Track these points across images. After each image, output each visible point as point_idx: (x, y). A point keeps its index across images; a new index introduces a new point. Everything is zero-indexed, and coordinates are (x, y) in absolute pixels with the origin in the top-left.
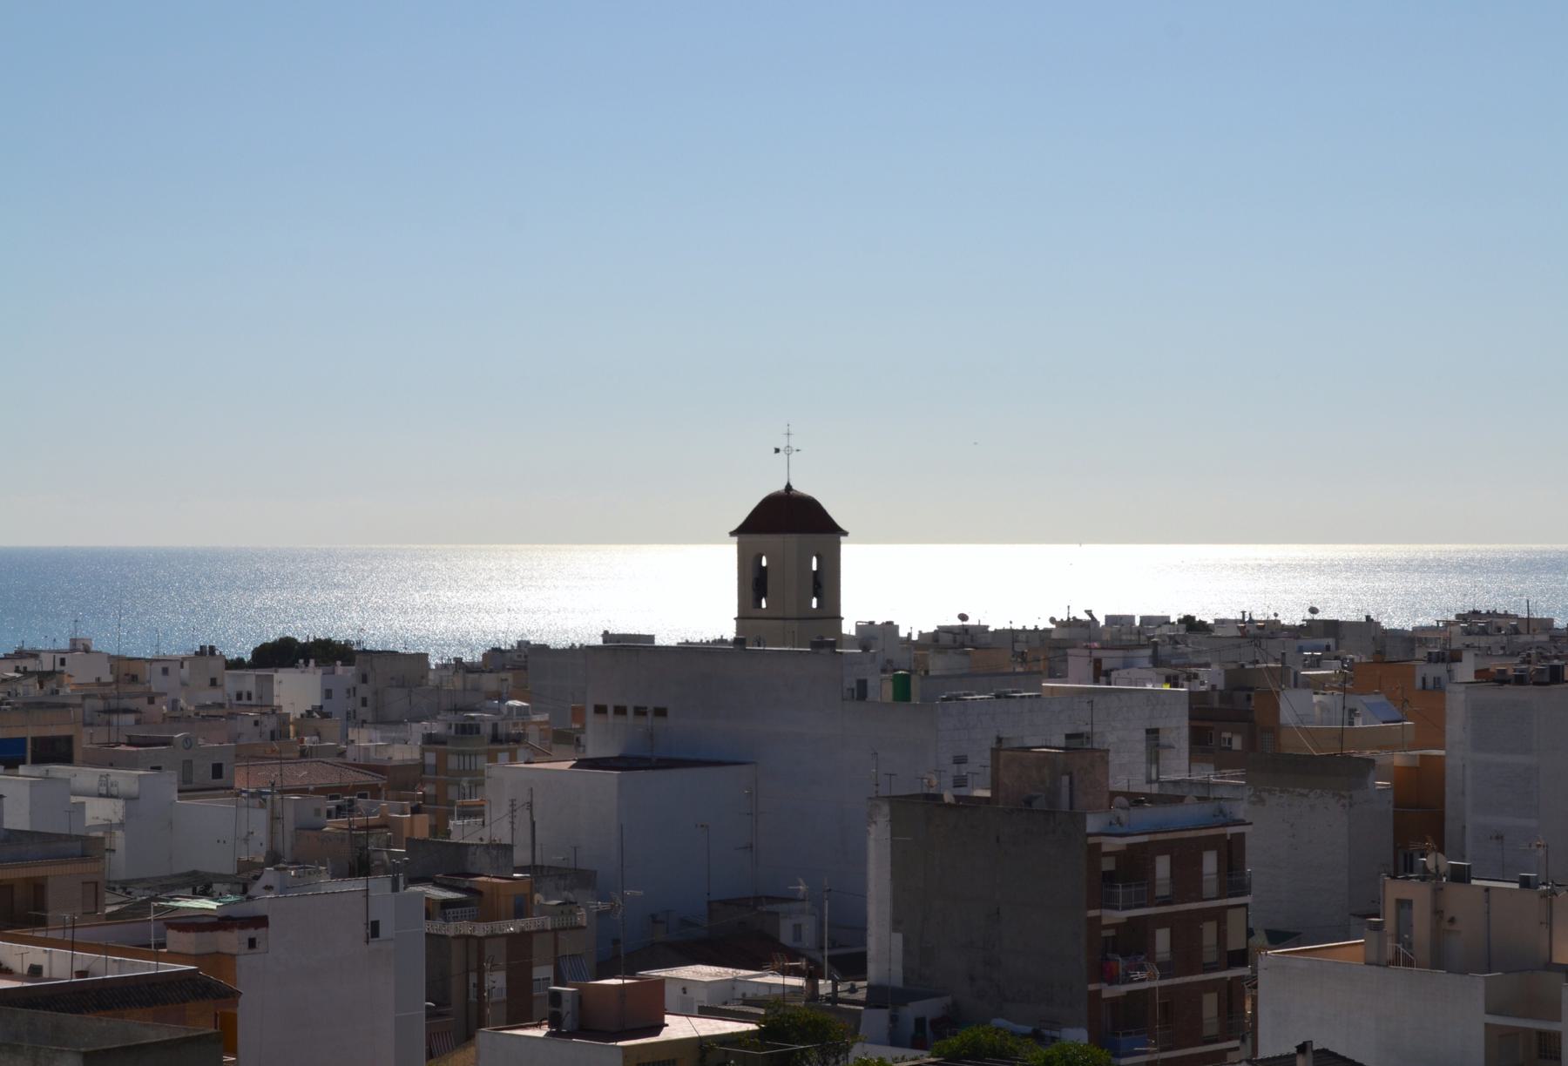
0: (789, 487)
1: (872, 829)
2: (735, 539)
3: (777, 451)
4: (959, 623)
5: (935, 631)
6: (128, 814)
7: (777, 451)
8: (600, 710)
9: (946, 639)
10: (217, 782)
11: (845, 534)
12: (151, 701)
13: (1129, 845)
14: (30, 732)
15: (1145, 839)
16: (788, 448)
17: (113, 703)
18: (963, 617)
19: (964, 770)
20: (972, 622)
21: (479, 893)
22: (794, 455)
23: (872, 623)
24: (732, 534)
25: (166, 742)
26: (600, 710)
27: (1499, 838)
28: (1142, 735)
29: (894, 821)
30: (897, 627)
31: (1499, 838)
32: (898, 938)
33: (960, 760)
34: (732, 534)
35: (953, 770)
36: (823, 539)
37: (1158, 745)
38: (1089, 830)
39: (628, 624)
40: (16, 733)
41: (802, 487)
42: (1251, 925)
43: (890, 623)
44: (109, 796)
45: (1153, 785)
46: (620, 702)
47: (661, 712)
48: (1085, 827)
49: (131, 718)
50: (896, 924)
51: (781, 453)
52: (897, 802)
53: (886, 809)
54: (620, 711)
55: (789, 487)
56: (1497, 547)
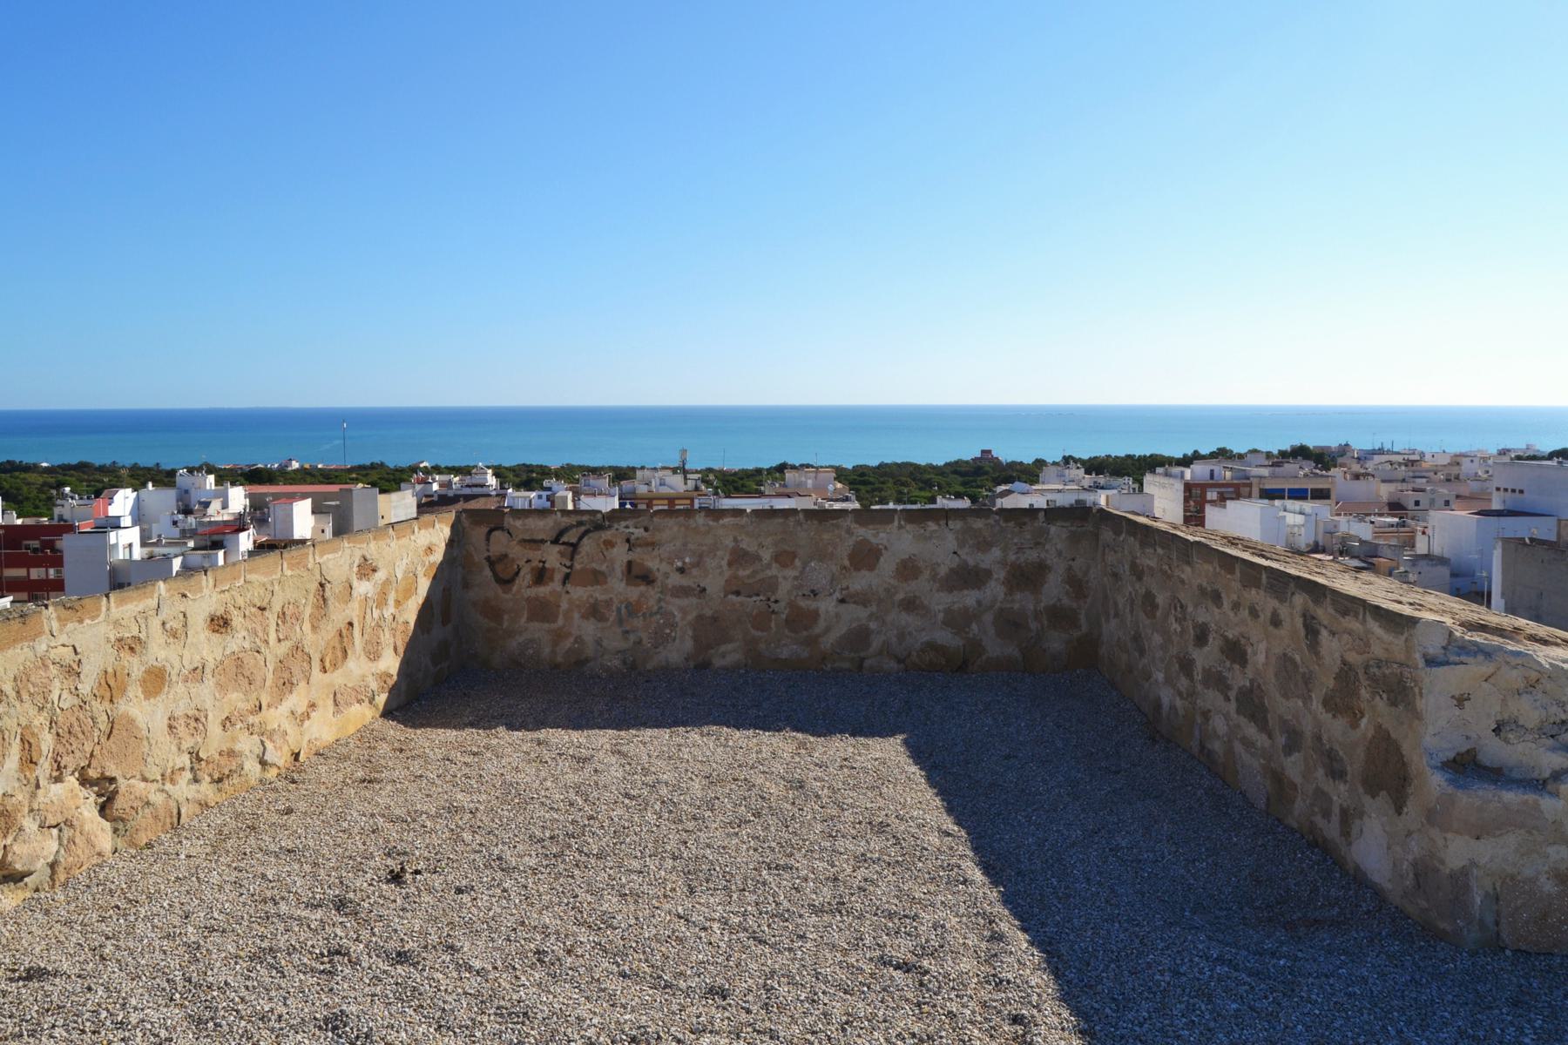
1: (1495, 552)
5: (975, 460)
6: (1306, 521)
8: (1498, 489)
10: (1417, 508)
12: (1436, 474)
14: (1287, 486)
17: (1417, 474)
21: (1374, 565)
25: (1423, 491)
26: (1498, 489)
29: (1504, 549)
32: (1503, 601)
39: (1131, 453)
40: (1305, 487)
44: (1301, 513)
45: (1425, 552)
47: (1521, 492)
49: (1424, 480)
50: (1503, 595)
52: (1506, 541)
53: (1500, 543)
54: (1506, 490)
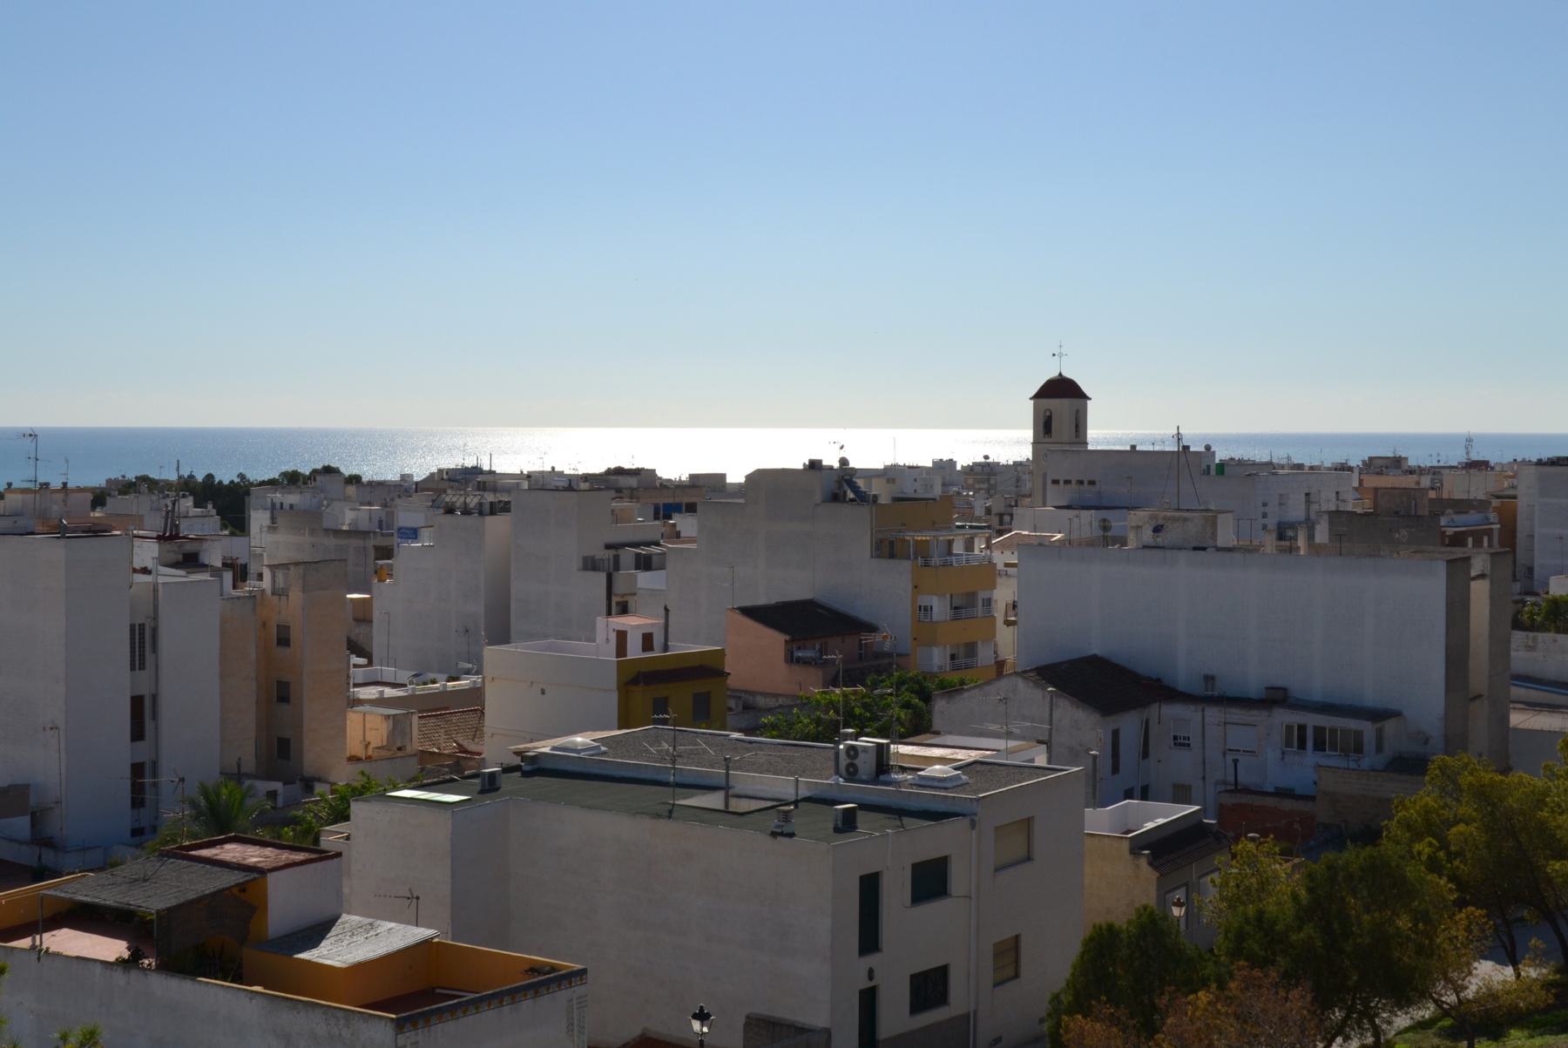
0: (1060, 374)
2: (1032, 402)
3: (1054, 355)
4: (983, 460)
7: (1054, 355)
8: (1055, 482)
9: (978, 469)
11: (1090, 399)
13: (1455, 532)
15: (1464, 529)
16: (1061, 355)
18: (986, 457)
19: (1267, 509)
20: (990, 460)
22: (1063, 358)
23: (941, 460)
24: (1031, 399)
26: (1055, 482)
27: (1561, 538)
28: (1334, 494)
29: (1331, 523)
30: (955, 462)
31: (1561, 538)
33: (1265, 505)
34: (1031, 399)
35: (1262, 509)
36: (1076, 402)
37: (1309, 501)
38: (1442, 524)
41: (1067, 374)
42: (367, 739)
43: (951, 460)
46: (1068, 478)
47: (1092, 483)
48: (1439, 523)
51: (1057, 356)
53: (1326, 517)
54: (1067, 482)
55: (1060, 374)
56: (1114, 431)
